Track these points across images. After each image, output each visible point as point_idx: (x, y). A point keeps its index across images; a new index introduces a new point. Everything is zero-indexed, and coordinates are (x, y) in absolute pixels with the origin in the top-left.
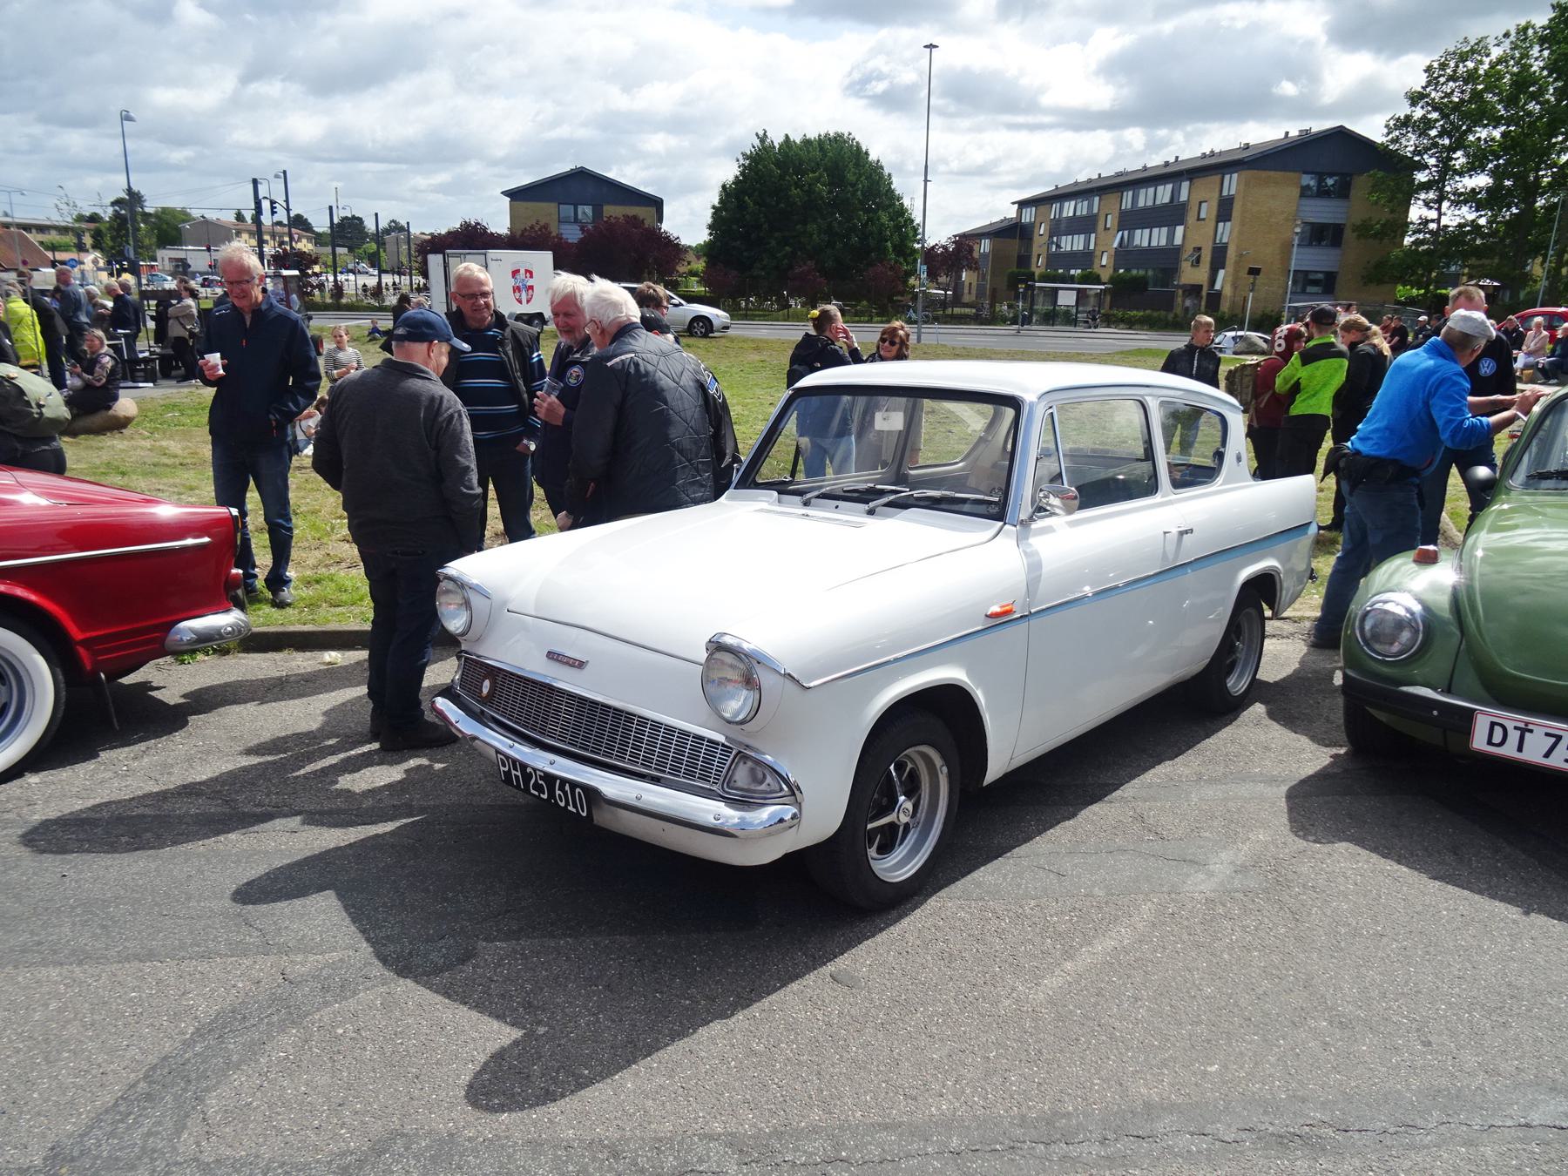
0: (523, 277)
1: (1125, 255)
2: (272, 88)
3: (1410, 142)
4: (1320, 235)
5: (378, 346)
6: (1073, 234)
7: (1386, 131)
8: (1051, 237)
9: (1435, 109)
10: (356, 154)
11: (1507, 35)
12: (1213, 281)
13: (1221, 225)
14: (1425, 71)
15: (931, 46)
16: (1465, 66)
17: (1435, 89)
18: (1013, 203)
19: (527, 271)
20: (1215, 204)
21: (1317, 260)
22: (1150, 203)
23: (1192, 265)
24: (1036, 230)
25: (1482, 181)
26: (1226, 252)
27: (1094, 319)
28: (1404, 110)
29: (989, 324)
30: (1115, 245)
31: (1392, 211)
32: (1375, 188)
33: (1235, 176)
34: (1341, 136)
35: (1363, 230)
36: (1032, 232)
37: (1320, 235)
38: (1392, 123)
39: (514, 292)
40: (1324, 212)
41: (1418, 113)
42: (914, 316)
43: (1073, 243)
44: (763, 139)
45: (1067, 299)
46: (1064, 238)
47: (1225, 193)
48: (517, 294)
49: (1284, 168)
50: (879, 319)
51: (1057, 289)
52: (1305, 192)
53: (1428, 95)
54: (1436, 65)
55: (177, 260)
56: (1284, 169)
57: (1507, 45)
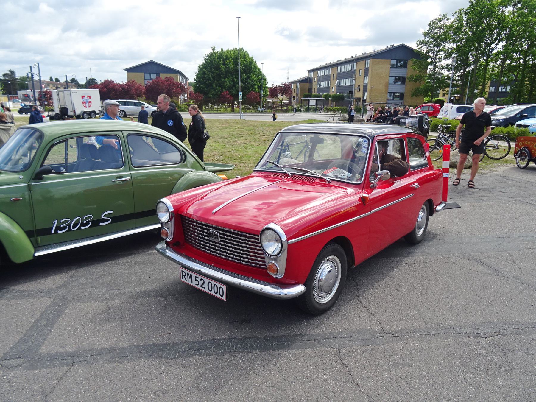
0: (87, 98)
1: (339, 87)
2: (73, 34)
3: (424, 49)
4: (401, 80)
5: (365, 119)
6: (324, 81)
7: (417, 45)
8: (318, 82)
9: (431, 38)
10: (103, 57)
11: (456, 13)
12: (364, 97)
13: (366, 77)
14: (429, 25)
15: (238, 18)
16: (440, 24)
17: (431, 31)
18: (307, 71)
19: (88, 96)
20: (363, 70)
21: (398, 89)
22: (345, 70)
23: (358, 91)
24: (313, 80)
25: (449, 61)
26: (367, 87)
27: (322, 110)
28: (422, 38)
29: (287, 112)
30: (336, 85)
31: (420, 72)
32: (414, 64)
33: (369, 61)
34: (403, 48)
35: (411, 78)
36: (312, 80)
37: (401, 80)
38: (418, 42)
39: (83, 103)
40: (400, 72)
41: (427, 39)
42: (260, 110)
43: (324, 84)
44: (213, 49)
45: (313, 103)
46: (321, 82)
47: (366, 67)
48: (84, 105)
49: (385, 58)
50: (249, 111)
51: (309, 100)
52: (393, 66)
53: (430, 33)
54: (431, 23)
55: (25, 94)
56: (385, 58)
57: (456, 16)
